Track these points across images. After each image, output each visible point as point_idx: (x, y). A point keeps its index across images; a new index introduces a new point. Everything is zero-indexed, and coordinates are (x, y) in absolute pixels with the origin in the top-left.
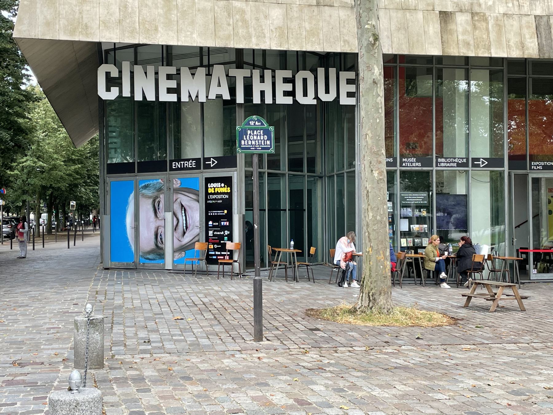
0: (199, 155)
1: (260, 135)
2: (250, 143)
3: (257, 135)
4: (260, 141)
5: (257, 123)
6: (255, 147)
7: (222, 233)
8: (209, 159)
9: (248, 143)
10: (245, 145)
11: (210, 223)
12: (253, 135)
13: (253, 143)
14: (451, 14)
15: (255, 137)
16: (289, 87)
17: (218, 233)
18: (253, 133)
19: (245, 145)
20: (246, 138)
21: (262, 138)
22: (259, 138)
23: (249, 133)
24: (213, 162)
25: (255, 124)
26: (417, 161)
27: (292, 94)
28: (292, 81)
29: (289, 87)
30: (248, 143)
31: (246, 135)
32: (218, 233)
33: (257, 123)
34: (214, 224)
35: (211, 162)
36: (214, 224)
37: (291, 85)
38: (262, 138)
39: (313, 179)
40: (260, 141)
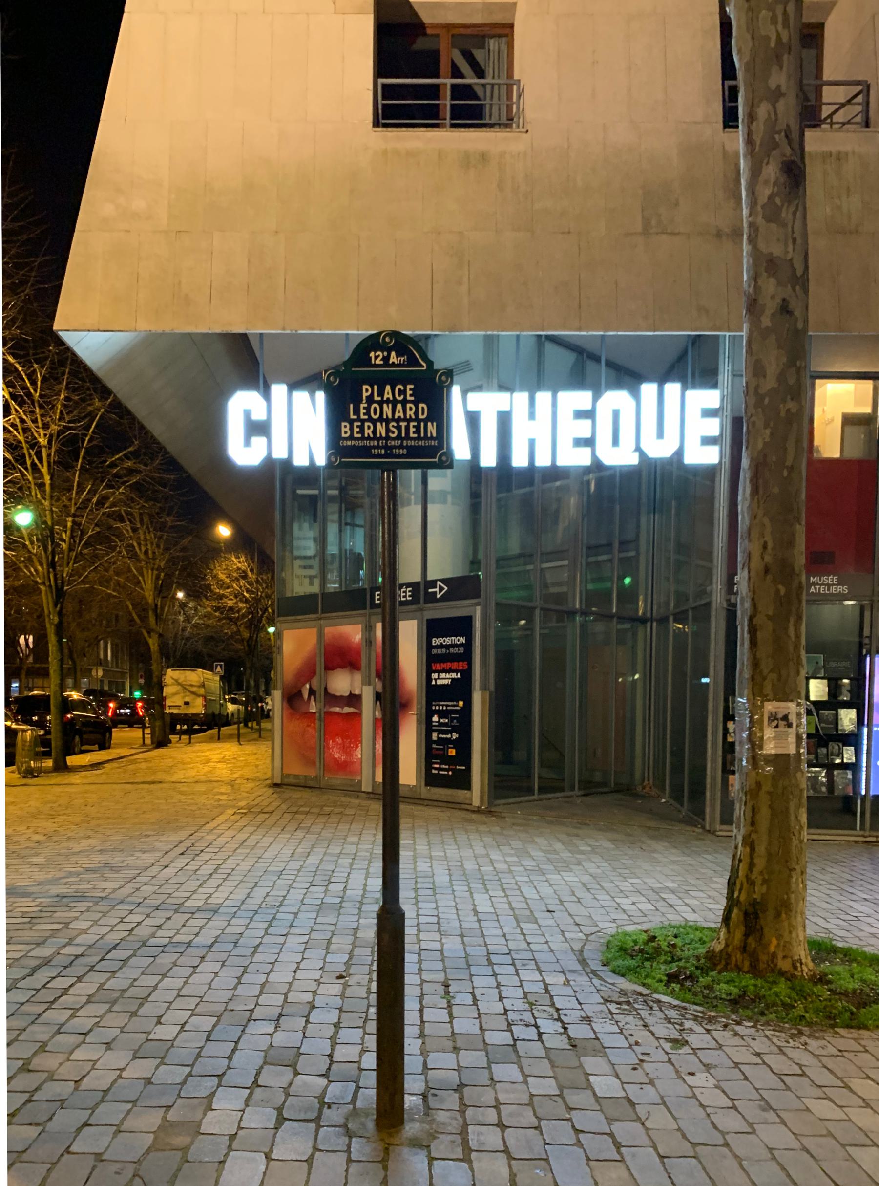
0: (417, 577)
1: (404, 402)
2: (368, 432)
3: (394, 403)
4: (403, 424)
5: (393, 358)
6: (386, 447)
7: (449, 736)
8: (433, 584)
9: (362, 431)
10: (351, 438)
11: (435, 718)
12: (381, 403)
13: (381, 429)
14: (838, 159)
15: (387, 410)
16: (583, 429)
17: (444, 736)
18: (381, 393)
19: (351, 438)
20: (357, 411)
21: (410, 413)
22: (399, 413)
23: (365, 395)
24: (441, 589)
25: (386, 359)
26: (765, 443)
27: (589, 442)
28: (589, 414)
29: (583, 429)
30: (362, 431)
31: (357, 401)
32: (444, 736)
33: (393, 358)
34: (442, 721)
35: (437, 590)
36: (442, 721)
37: (588, 422)
38: (410, 413)
39: (627, 626)
40: (403, 424)
